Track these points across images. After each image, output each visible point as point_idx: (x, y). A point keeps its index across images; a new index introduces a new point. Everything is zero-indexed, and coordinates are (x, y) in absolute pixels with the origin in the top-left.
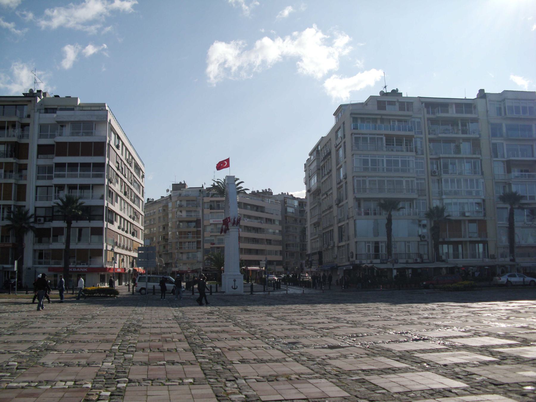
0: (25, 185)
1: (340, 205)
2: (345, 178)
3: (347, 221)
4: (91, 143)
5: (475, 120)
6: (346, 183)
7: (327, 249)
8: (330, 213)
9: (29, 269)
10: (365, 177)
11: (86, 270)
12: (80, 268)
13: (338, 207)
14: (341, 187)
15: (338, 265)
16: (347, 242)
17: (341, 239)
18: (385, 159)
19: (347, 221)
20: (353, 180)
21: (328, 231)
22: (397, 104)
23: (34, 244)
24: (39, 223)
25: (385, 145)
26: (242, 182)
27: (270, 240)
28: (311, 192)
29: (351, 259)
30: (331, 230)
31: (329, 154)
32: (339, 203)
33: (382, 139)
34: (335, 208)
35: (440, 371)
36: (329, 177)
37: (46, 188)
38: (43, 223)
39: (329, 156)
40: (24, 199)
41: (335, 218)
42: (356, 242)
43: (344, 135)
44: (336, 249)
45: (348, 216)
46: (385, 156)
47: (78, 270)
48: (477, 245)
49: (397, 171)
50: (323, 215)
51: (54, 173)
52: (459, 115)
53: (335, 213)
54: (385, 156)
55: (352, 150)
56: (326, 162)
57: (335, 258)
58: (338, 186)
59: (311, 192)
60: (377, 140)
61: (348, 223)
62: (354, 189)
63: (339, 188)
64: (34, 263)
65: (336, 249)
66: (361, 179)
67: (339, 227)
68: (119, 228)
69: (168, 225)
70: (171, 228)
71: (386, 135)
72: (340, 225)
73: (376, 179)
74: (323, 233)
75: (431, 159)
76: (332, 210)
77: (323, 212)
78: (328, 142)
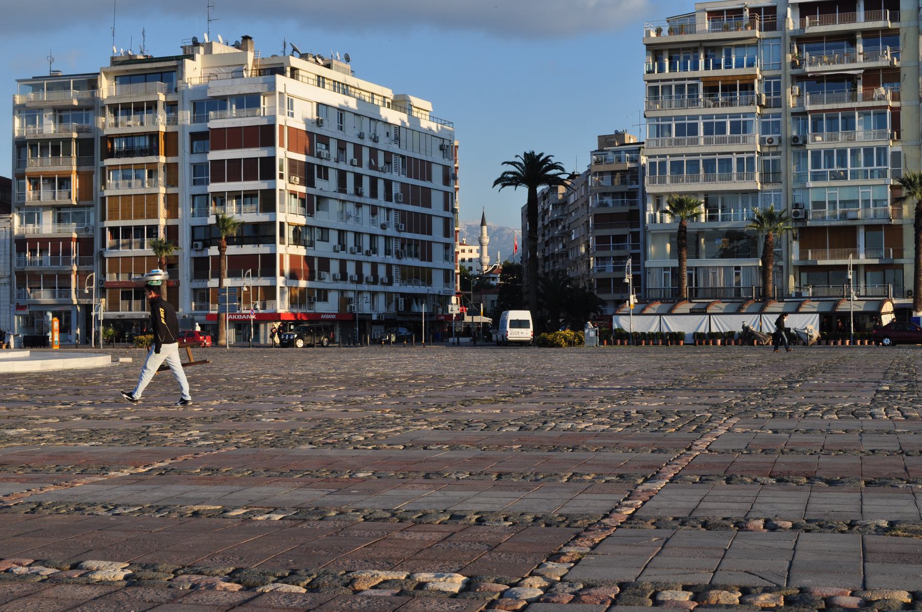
10: (665, 156)
24: (197, 250)
38: (202, 250)
46: (700, 117)
51: (822, 169)
54: (700, 117)
73: (685, 159)
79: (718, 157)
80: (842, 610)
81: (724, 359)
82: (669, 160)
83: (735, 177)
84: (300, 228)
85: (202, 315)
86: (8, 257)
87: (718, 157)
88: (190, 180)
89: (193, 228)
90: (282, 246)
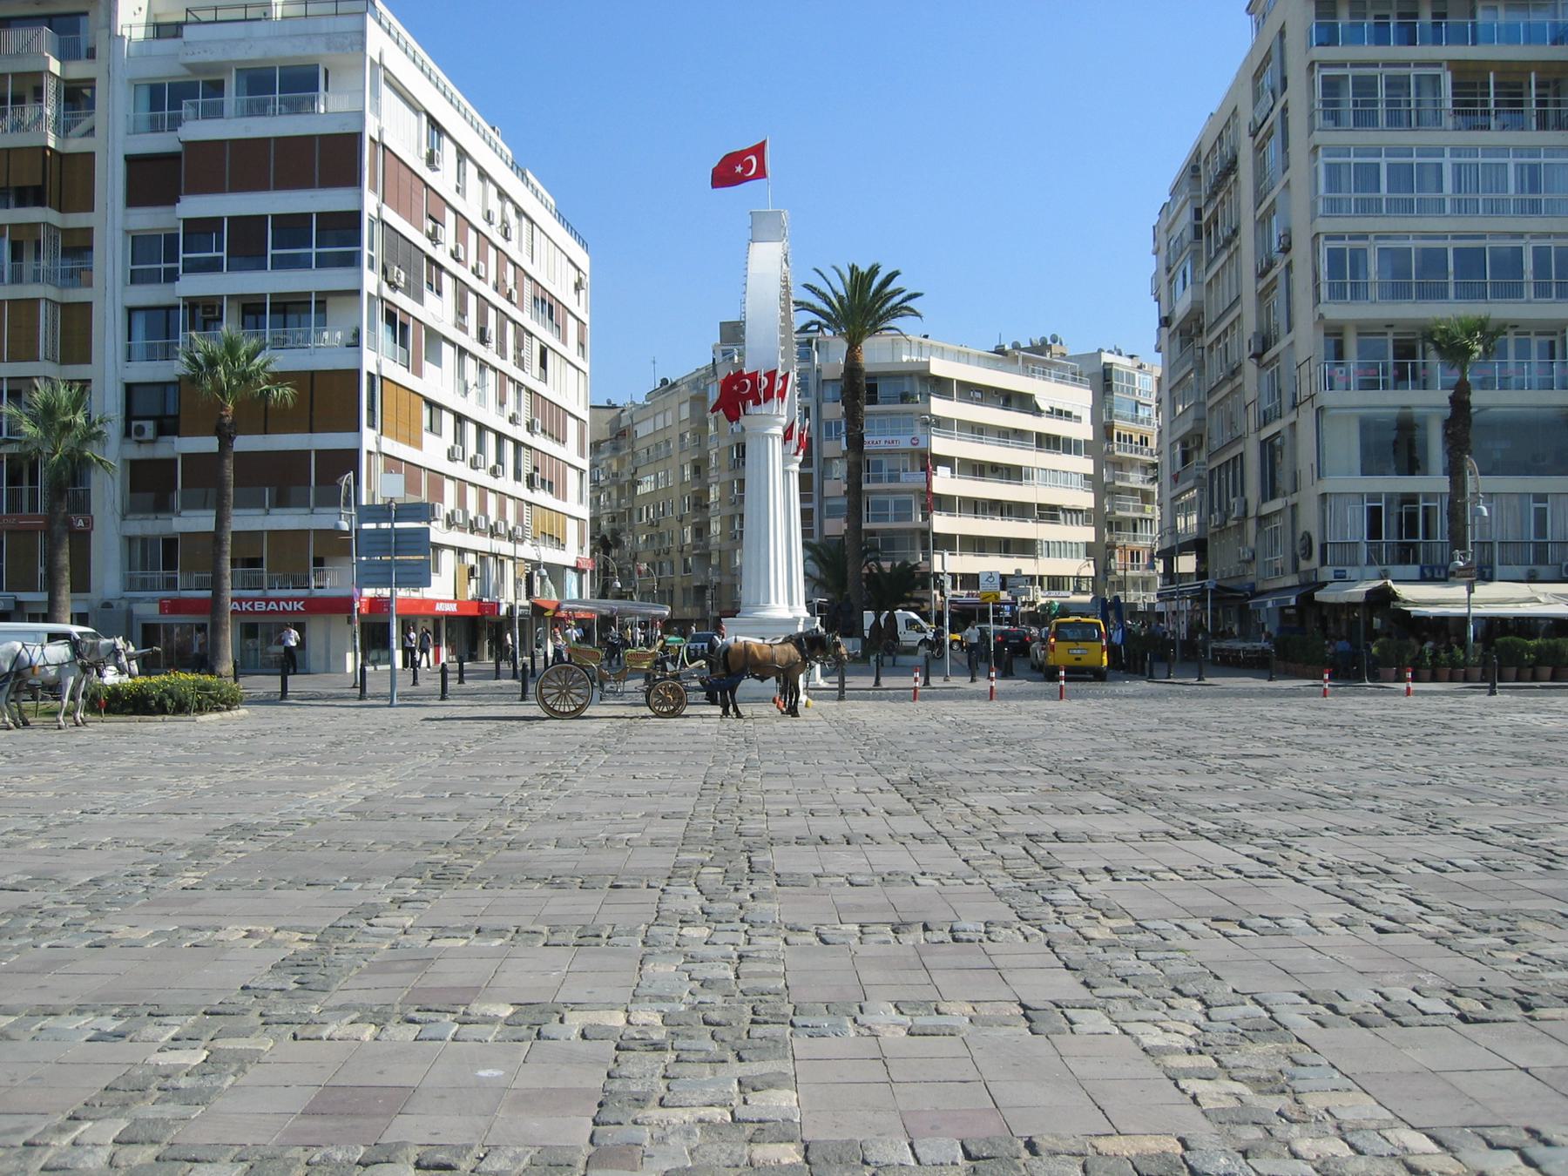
0: (87, 306)
1: (1267, 357)
2: (1286, 250)
3: (1292, 418)
6: (1289, 267)
7: (1223, 528)
8: (1233, 391)
9: (107, 605)
10: (1364, 236)
11: (299, 606)
12: (278, 600)
13: (1262, 366)
14: (1272, 286)
15: (1260, 587)
16: (1291, 500)
17: (1270, 490)
18: (1447, 163)
19: (1292, 418)
20: (1315, 251)
21: (1227, 462)
23: (123, 517)
24: (140, 442)
25: (1448, 105)
26: (894, 274)
28: (1174, 326)
29: (1304, 565)
30: (1235, 458)
31: (1231, 167)
32: (1265, 350)
33: (1436, 79)
34: (1250, 367)
36: (1230, 257)
37: (164, 312)
38: (153, 442)
39: (1232, 177)
40: (86, 359)
41: (1251, 408)
42: (1324, 496)
43: (1284, 81)
44: (1251, 525)
45: (1295, 395)
46: (1447, 152)
47: (273, 606)
49: (1495, 208)
50: (1210, 403)
51: (181, 256)
53: (1250, 393)
54: (1447, 152)
55: (1311, 130)
56: (1222, 202)
57: (1248, 562)
58: (1262, 285)
59: (1174, 326)
60: (1418, 86)
61: (1293, 425)
62: (1317, 287)
63: (1263, 295)
64: (130, 585)
65: (1251, 525)
67: (1263, 443)
68: (451, 456)
69: (707, 460)
70: (717, 468)
71: (1457, 67)
72: (1267, 433)
74: (1212, 471)
76: (1238, 380)
77: (1212, 392)
78: (1227, 126)
80: (790, 1154)
83: (1529, 291)
84: (1449, 432)
85: (153, 600)
88: (124, 270)
89: (130, 388)
90: (371, 431)
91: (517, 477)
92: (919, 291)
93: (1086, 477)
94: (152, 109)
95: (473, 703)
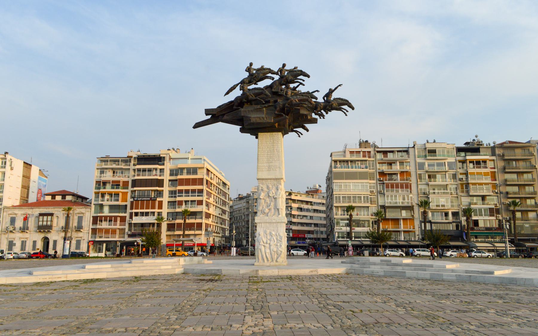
4: (196, 179)
5: (483, 144)
10: (340, 194)
11: (192, 245)
22: (361, 153)
27: (317, 224)
35: (465, 326)
48: (516, 224)
52: (110, 227)
66: (338, 195)
73: (346, 195)
75: (379, 184)
79: (357, 196)
81: (355, 278)
82: (341, 196)
86: (89, 223)
87: (357, 196)
91: (218, 204)
92: (353, 104)
93: (325, 218)
94: (189, 196)
95: (377, 273)
